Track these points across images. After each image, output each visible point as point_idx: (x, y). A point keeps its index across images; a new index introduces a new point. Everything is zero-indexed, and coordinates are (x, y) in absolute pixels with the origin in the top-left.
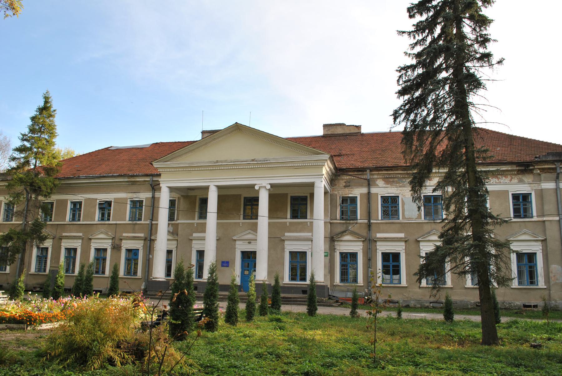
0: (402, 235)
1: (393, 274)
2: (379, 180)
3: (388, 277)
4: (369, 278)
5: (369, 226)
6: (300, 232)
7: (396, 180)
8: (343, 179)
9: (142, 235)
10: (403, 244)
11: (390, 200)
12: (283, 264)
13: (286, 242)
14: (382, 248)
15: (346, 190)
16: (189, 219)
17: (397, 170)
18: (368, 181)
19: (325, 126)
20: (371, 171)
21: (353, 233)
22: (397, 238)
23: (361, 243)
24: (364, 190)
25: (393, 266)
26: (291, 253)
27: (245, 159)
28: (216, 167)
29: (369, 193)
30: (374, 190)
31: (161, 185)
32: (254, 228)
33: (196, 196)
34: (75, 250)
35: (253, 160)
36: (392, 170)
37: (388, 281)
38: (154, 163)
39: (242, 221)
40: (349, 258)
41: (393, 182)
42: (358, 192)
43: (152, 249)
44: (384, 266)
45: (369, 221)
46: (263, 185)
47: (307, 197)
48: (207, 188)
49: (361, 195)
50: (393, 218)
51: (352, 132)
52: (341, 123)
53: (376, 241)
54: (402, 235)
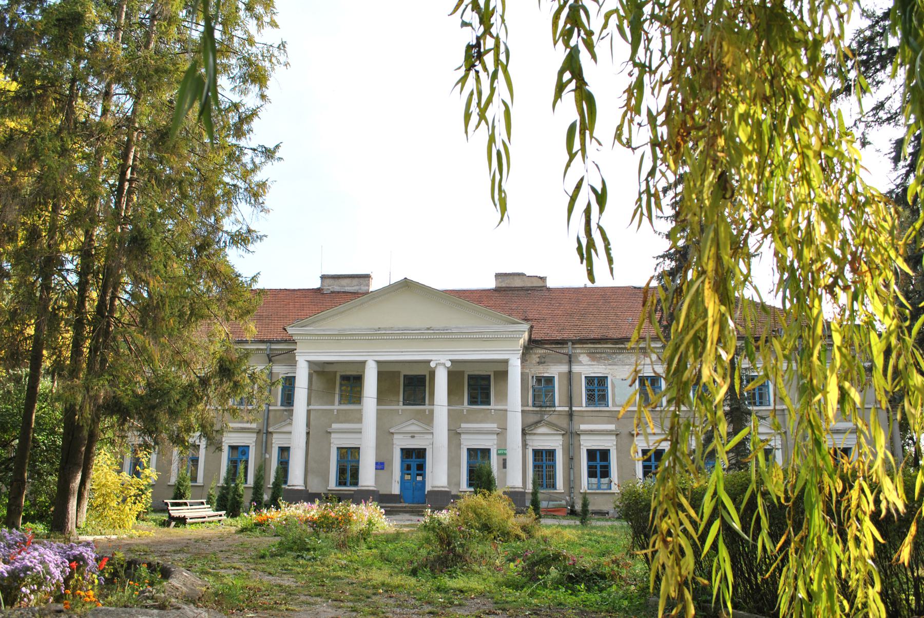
0: (612, 427)
1: (601, 477)
2: (582, 356)
3: (594, 480)
4: (571, 483)
5: (571, 414)
6: (481, 422)
7: (603, 355)
8: (535, 354)
9: (254, 425)
10: (614, 438)
11: (596, 382)
12: (459, 466)
13: (463, 436)
14: (588, 443)
15: (541, 367)
16: (327, 404)
17: (606, 343)
18: (570, 356)
19: (498, 276)
20: (573, 344)
21: (550, 424)
22: (607, 431)
23: (561, 437)
24: (564, 368)
25: (601, 467)
26: (470, 450)
27: (418, 326)
28: (377, 336)
29: (570, 372)
30: (576, 369)
31: (297, 358)
32: (429, 419)
33: (336, 372)
34: (551, 453)
35: (428, 329)
36: (599, 343)
37: (595, 486)
38: (288, 329)
39: (401, 407)
40: (479, 455)
41: (601, 358)
42: (556, 370)
43: (269, 446)
44: (589, 467)
45: (571, 408)
46: (440, 361)
47: (490, 376)
48: (363, 363)
49: (560, 374)
50: (600, 405)
51: (535, 285)
52: (520, 271)
53: (579, 435)
54: (612, 427)
